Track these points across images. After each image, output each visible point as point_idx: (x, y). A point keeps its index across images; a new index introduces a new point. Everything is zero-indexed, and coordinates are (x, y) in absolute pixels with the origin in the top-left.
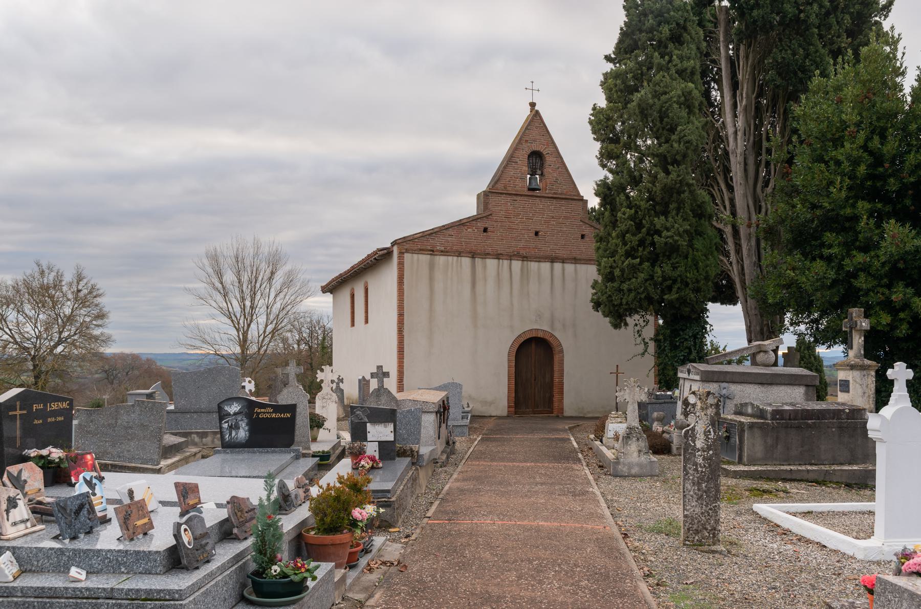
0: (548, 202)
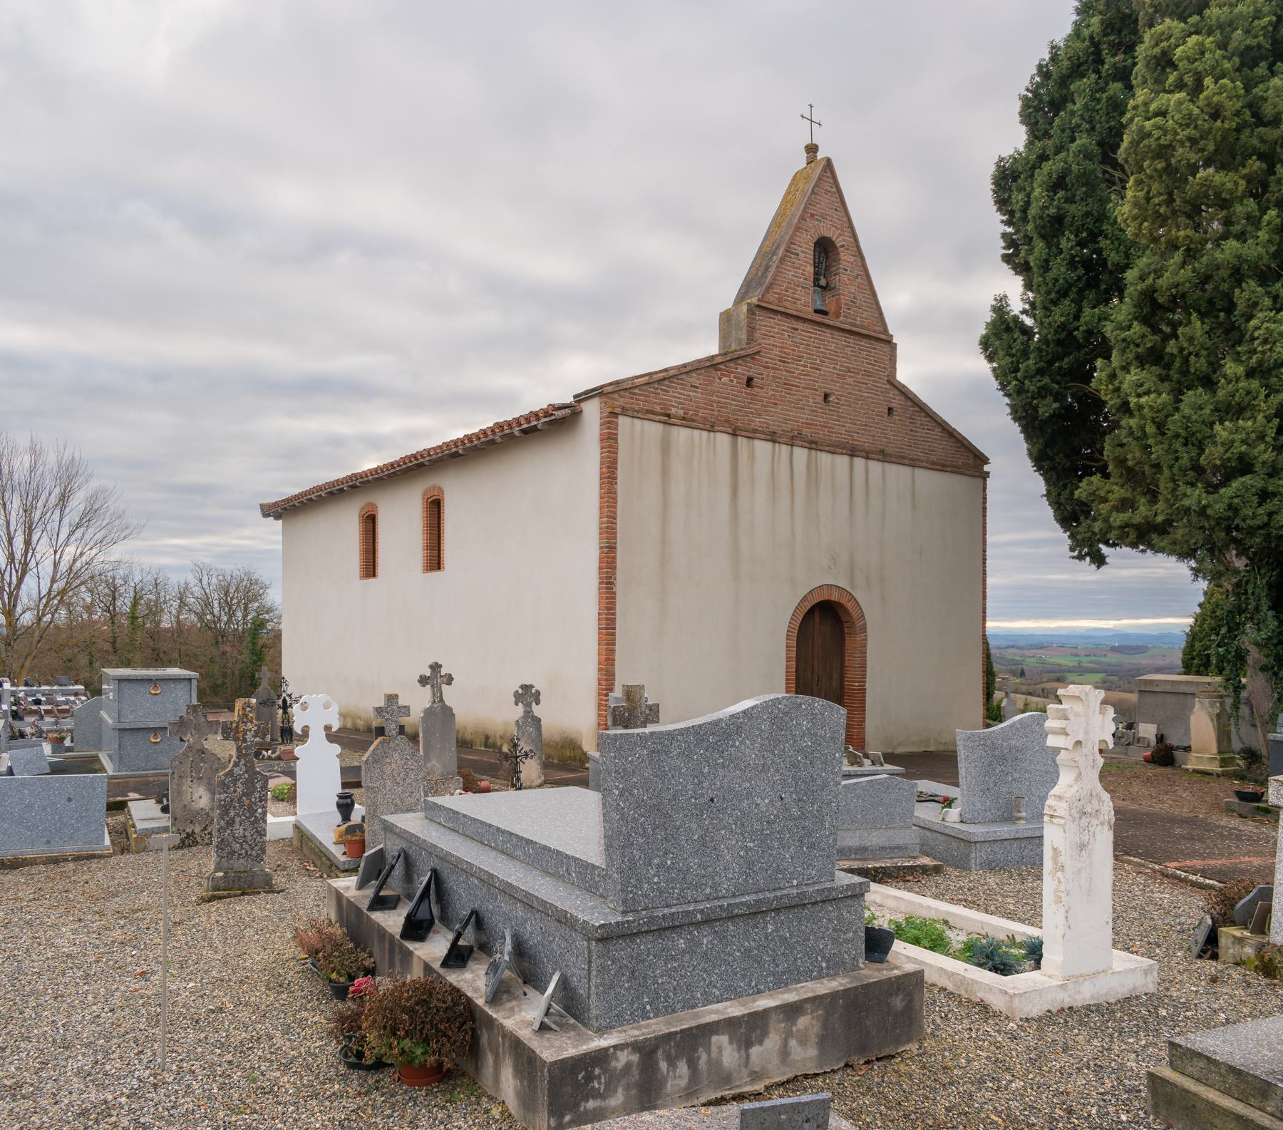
0: (842, 339)
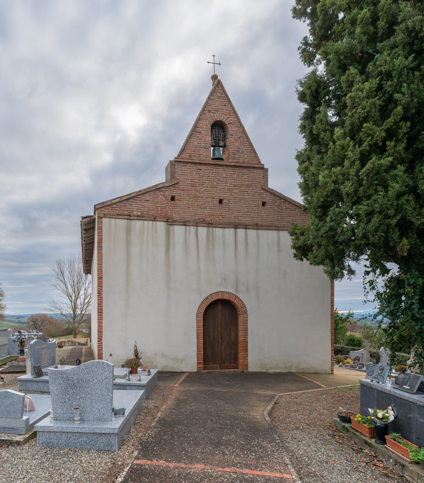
0: (230, 171)
